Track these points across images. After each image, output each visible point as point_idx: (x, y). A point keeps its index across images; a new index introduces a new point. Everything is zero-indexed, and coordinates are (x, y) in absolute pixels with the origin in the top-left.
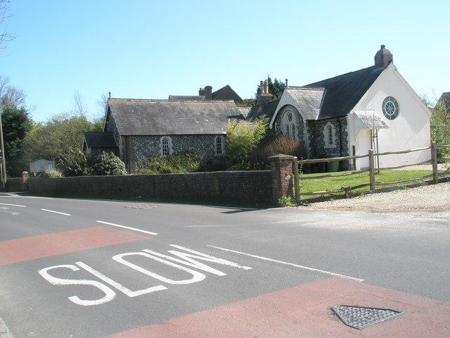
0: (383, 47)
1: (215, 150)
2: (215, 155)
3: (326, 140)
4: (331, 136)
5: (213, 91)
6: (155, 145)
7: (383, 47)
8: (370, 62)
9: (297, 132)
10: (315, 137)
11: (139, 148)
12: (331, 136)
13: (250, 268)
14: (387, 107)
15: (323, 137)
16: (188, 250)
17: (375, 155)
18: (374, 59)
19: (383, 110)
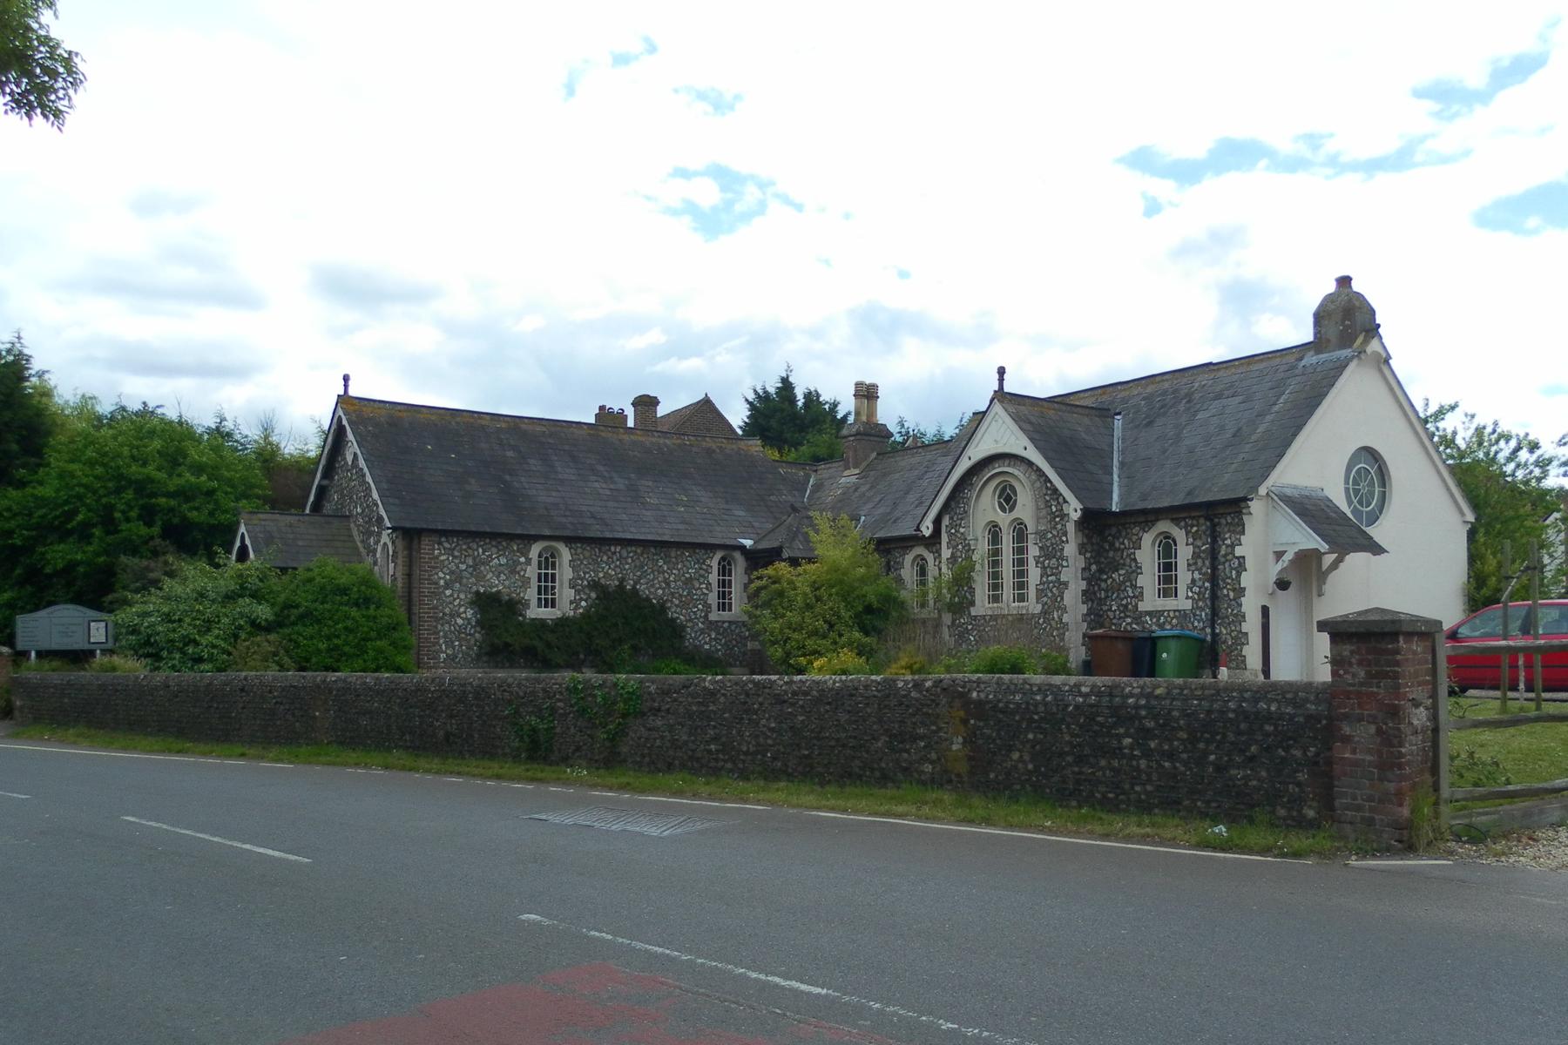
0: (1344, 282)
1: (713, 599)
2: (713, 617)
3: (1148, 579)
4: (1168, 567)
5: (661, 411)
6: (513, 569)
7: (1344, 282)
8: (1289, 328)
9: (1033, 551)
10: (1101, 571)
11: (457, 577)
12: (1168, 567)
13: (525, 917)
14: (1355, 482)
15: (1138, 570)
16: (351, 383)
17: (1538, 708)
18: (1310, 320)
19: (1347, 490)
